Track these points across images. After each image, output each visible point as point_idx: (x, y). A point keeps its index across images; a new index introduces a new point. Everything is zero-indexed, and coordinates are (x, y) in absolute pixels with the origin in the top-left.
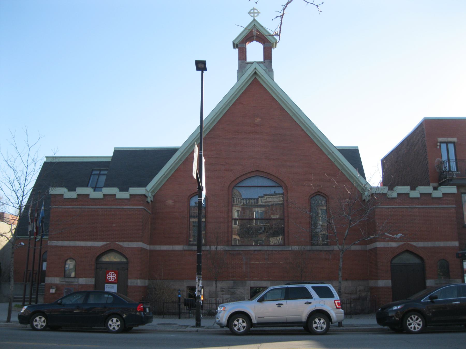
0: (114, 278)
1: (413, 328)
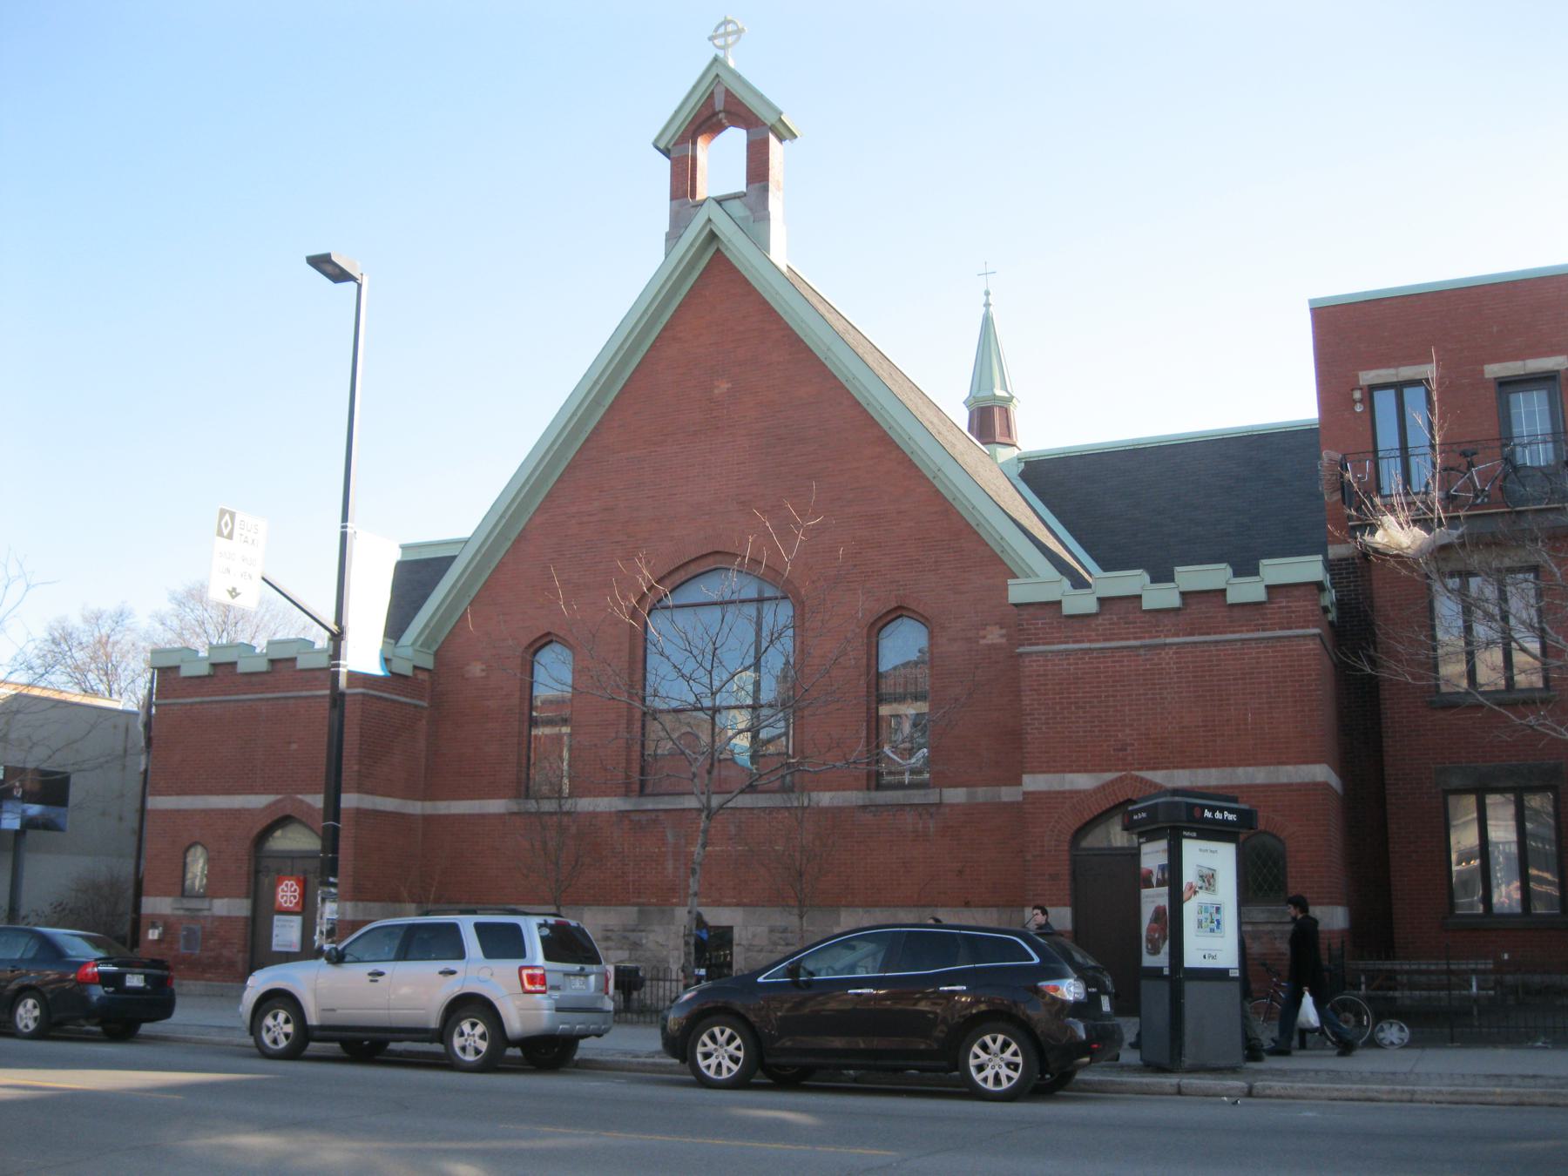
0: (295, 897)
1: (991, 1080)
